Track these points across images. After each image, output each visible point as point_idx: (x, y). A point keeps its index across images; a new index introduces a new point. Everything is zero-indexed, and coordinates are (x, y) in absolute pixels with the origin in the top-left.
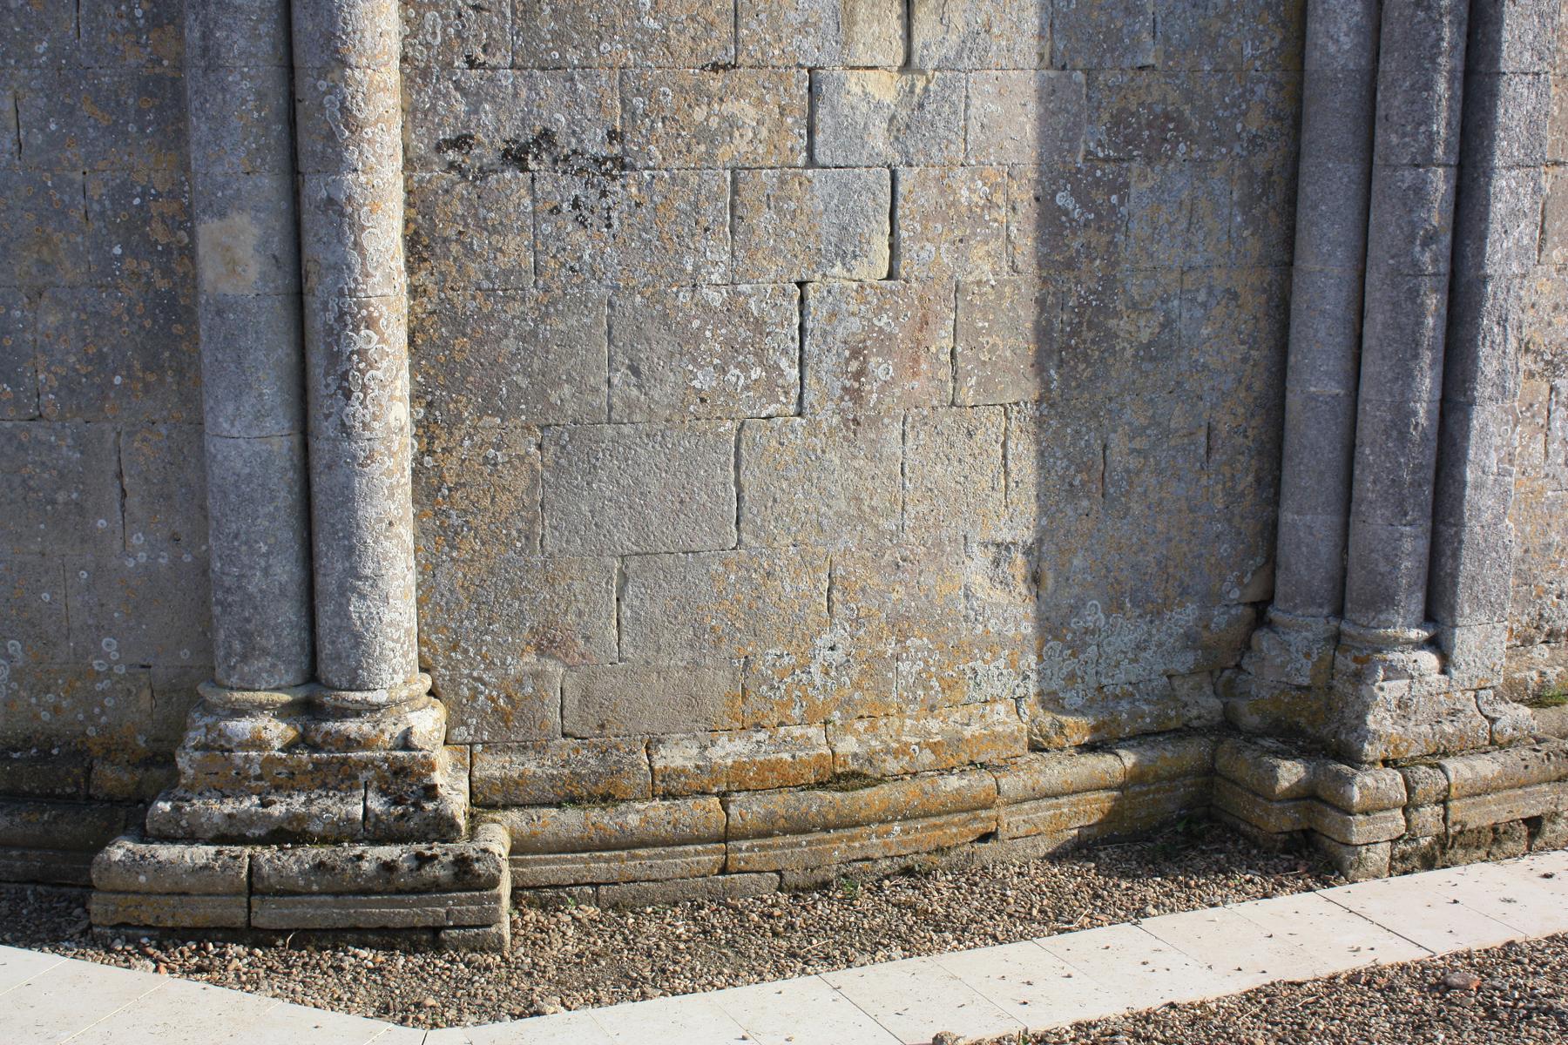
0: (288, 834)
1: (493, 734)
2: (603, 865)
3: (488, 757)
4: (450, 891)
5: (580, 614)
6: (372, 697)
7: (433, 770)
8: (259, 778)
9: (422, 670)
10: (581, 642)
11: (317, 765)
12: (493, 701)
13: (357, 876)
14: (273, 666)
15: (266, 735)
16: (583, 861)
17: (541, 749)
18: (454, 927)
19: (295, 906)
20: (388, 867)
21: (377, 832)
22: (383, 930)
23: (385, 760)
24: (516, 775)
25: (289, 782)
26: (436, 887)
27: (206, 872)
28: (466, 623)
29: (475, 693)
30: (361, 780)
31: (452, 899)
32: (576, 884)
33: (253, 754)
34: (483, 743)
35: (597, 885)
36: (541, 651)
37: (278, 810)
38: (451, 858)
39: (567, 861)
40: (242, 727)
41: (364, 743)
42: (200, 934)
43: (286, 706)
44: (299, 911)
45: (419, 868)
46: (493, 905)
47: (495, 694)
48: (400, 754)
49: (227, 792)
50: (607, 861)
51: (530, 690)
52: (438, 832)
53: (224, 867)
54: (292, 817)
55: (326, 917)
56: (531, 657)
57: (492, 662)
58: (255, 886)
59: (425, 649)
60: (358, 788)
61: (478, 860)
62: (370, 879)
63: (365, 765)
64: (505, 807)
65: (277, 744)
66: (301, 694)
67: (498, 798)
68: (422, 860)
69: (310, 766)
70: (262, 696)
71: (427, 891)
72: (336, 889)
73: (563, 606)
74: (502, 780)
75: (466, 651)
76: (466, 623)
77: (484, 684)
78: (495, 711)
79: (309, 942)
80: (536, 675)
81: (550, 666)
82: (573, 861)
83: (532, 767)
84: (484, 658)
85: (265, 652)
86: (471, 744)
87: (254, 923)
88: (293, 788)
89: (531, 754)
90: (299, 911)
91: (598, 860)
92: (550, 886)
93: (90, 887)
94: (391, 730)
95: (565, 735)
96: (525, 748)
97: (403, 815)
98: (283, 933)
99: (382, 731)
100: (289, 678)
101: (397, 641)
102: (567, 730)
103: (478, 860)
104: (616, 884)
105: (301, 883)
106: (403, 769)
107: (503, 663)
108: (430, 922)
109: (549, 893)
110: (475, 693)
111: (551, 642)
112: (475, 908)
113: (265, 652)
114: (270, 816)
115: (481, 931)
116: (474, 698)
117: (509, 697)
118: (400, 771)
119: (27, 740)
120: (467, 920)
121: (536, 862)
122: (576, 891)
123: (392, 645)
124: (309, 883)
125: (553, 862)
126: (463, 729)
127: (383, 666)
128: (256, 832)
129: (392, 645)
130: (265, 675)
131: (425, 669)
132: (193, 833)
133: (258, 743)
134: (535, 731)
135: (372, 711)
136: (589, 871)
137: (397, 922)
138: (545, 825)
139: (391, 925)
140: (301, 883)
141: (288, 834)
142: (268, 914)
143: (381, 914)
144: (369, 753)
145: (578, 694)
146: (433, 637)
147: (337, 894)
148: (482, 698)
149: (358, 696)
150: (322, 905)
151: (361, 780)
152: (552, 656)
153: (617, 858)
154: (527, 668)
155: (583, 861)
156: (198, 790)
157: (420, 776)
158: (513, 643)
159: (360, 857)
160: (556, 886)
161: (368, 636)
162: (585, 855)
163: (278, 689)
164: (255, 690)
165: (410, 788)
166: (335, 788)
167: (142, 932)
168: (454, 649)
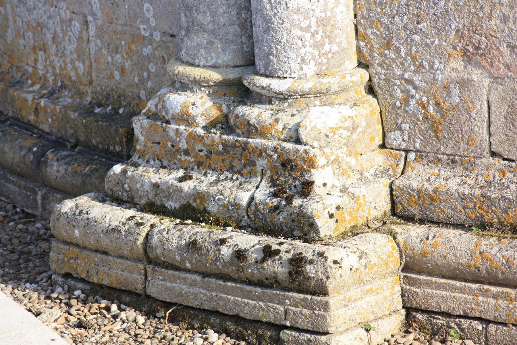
0: (192, 211)
1: (426, 143)
2: (492, 301)
3: (419, 167)
4: (290, 290)
5: (505, 20)
6: (278, 85)
7: (313, 166)
8: (187, 153)
9: (360, 64)
10: (506, 52)
11: (225, 145)
12: (424, 107)
13: (217, 259)
14: (210, 43)
15: (193, 111)
16: (471, 292)
17: (469, 166)
18: (291, 328)
19: (175, 281)
20: (240, 255)
21: (255, 221)
22: (237, 319)
23: (275, 149)
24: (430, 189)
25: (204, 160)
26: (270, 283)
27: (116, 235)
28: (397, 18)
29: (407, 98)
30: (259, 168)
31: (288, 298)
32: (465, 317)
33: (182, 128)
34: (417, 151)
35: (488, 322)
36: (467, 58)
37: (187, 186)
38: (290, 256)
39: (456, 289)
40: (177, 100)
41: (258, 131)
42: (98, 292)
43: (218, 84)
44: (177, 285)
45: (263, 260)
46: (322, 313)
47: (424, 99)
48: (289, 146)
49: (165, 163)
50: (495, 297)
51: (457, 100)
52: (301, 229)
53: (128, 232)
54: (198, 195)
55: (196, 296)
56: (458, 63)
57: (421, 65)
58: (150, 257)
59: (362, 44)
60: (256, 176)
61: (311, 262)
62: (225, 265)
63: (261, 152)
64: (422, 222)
65: (202, 121)
66: (232, 75)
67: (414, 211)
68: (268, 253)
69: (221, 147)
70: (196, 72)
71: (270, 286)
72: (203, 270)
73: (486, 9)
74: (419, 191)
75: (398, 50)
76: (397, 18)
77: (415, 88)
78: (426, 118)
79: (184, 319)
80: (464, 84)
81: (478, 76)
82: (462, 290)
83: (453, 185)
84: (414, 59)
85: (202, 29)
86: (407, 151)
87: (148, 292)
88: (210, 167)
89: (459, 170)
90: (177, 285)
91: (486, 293)
92: (424, 311)
93: (49, 237)
94: (287, 118)
95: (493, 154)
96: (454, 162)
97: (277, 208)
98: (167, 305)
99: (277, 121)
100: (226, 58)
101: (307, 30)
102: (494, 148)
103: (311, 262)
104: (505, 324)
105: (178, 258)
106: (289, 161)
107: (432, 67)
108: (271, 318)
109: (441, 321)
110: (407, 98)
111: (477, 48)
112: (306, 311)
113: (202, 29)
114: (181, 190)
115: (312, 337)
116: (406, 101)
117: (438, 104)
118: (287, 164)
119: (108, 97)
120: (301, 324)
121: (429, 285)
122: (465, 323)
123: (300, 33)
124: (183, 260)
125: (443, 287)
126: (398, 133)
127: (291, 54)
128: (172, 204)
129: (300, 33)
130: (203, 51)
131: (363, 64)
132: (133, 198)
133: (185, 118)
134: (463, 145)
135: (280, 100)
136: (477, 304)
137: (246, 313)
138: (434, 247)
139: (242, 315)
140: (178, 258)
141: (192, 211)
142: (160, 285)
143: (235, 302)
144: (264, 141)
145: (504, 109)
146: (369, 31)
147: (205, 275)
148: (413, 103)
149: (264, 81)
150: (194, 284)
151: (259, 168)
152: (478, 65)
153: (505, 296)
154: (453, 75)
155: (471, 292)
156: (147, 157)
157: (303, 171)
158: (440, 46)
159: (223, 242)
160: (447, 315)
161: (276, 21)
162: (474, 286)
163: (215, 67)
164: (192, 65)
165: (292, 182)
166: (239, 172)
167: (80, 285)
168: (388, 45)
